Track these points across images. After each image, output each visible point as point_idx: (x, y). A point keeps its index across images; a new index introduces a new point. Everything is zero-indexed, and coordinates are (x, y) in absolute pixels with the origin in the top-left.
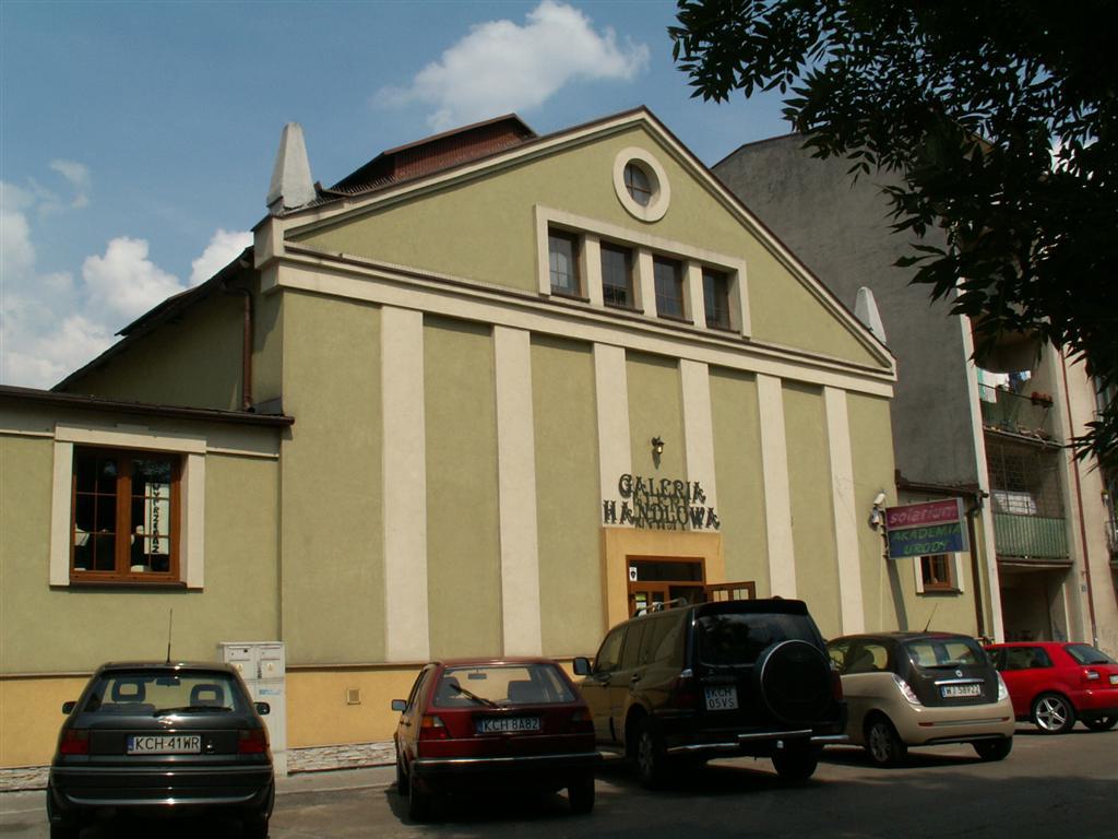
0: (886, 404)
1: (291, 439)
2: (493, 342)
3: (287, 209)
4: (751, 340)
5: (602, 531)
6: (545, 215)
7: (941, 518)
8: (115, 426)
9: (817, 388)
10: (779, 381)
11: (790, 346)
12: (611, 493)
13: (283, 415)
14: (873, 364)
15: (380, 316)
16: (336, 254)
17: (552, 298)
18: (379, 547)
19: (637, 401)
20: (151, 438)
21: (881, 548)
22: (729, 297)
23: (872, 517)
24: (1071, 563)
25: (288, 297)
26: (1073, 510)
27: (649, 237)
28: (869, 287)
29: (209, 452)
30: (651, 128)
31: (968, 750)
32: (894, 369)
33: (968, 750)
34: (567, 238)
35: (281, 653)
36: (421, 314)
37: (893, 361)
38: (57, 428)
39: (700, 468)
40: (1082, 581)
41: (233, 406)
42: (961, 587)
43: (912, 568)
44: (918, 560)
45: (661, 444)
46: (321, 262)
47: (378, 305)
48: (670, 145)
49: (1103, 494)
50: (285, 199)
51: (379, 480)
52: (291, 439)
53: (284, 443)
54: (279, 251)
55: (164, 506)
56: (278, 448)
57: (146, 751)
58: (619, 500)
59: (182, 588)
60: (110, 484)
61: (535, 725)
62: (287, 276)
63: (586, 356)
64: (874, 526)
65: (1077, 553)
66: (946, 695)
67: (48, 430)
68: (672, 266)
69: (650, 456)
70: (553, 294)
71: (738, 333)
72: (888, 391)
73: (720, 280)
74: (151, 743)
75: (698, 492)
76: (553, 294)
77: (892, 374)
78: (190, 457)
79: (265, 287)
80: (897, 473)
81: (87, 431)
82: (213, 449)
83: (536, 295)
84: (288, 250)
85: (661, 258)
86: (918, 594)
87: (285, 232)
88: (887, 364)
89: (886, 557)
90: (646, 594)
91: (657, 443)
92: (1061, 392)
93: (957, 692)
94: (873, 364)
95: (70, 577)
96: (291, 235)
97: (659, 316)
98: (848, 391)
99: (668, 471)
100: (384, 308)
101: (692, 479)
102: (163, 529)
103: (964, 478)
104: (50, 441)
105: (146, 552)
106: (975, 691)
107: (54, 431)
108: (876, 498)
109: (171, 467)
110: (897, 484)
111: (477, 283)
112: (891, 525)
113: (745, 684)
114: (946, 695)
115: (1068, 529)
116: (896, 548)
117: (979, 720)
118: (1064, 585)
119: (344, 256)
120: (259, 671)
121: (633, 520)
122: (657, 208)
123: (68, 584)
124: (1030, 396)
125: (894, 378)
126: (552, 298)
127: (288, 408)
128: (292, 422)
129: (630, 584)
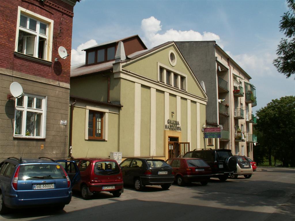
0: (205, 106)
1: (121, 110)
2: (164, 95)
3: (121, 61)
4: (187, 92)
5: (165, 131)
6: (160, 64)
7: (217, 131)
8: (95, 106)
9: (149, 88)
10: (169, 94)
11: (134, 72)
12: (166, 123)
13: (121, 105)
14: (204, 98)
15: (134, 85)
16: (129, 71)
17: (160, 82)
18: (134, 133)
19: (157, 99)
20: (100, 109)
21: (203, 136)
22: (183, 82)
23: (202, 129)
24: (229, 140)
25: (122, 80)
26: (231, 129)
27: (173, 70)
28: (204, 81)
29: (109, 112)
30: (175, 46)
31: (243, 176)
32: (207, 99)
33: (243, 176)
34: (162, 69)
35: (121, 154)
36: (140, 85)
37: (207, 97)
38: (87, 106)
39: (179, 120)
40: (231, 144)
41: (102, 100)
42: (214, 144)
43: (207, 140)
44: (208, 139)
45: (173, 113)
46: (127, 73)
47: (134, 82)
48: (176, 48)
49: (234, 126)
50: (121, 59)
51: (134, 119)
52: (121, 110)
53: (121, 111)
54: (121, 70)
55: (100, 123)
56: (119, 112)
57: (160, 174)
58: (167, 125)
59: (104, 140)
60: (249, 143)
61: (203, 170)
62: (122, 76)
63: (186, 101)
64: (202, 131)
65: (230, 138)
66: (244, 167)
67: (85, 107)
68: (176, 75)
69: (171, 116)
70: (160, 81)
71: (185, 90)
72: (205, 103)
73: (183, 78)
74: (161, 173)
75: (178, 124)
76: (160, 81)
77: (207, 100)
78: (106, 113)
79: (115, 76)
80: (206, 121)
81: (91, 107)
82: (110, 112)
83: (157, 81)
84: (123, 70)
85: (176, 75)
86: (207, 146)
87: (122, 66)
88: (206, 98)
89: (204, 138)
90: (171, 144)
91: (173, 113)
92: (230, 105)
93: (245, 166)
94: (204, 98)
95: (88, 138)
96: (123, 67)
97: (174, 86)
98: (200, 103)
99: (173, 119)
100: (135, 83)
101: (178, 121)
102: (100, 128)
103: (214, 122)
104: (85, 109)
105: (97, 133)
106: (248, 166)
107: (86, 107)
108: (203, 126)
109: (102, 114)
110: (206, 123)
111: (149, 79)
112: (205, 131)
113: (224, 164)
114: (244, 167)
115: (229, 133)
116: (205, 136)
117: (246, 171)
118: (227, 145)
119: (130, 72)
120: (118, 158)
121: (169, 129)
122: (174, 63)
123: (88, 139)
124: (225, 105)
125: (207, 101)
126: (160, 82)
127: (122, 103)
128: (123, 106)
129: (169, 142)
